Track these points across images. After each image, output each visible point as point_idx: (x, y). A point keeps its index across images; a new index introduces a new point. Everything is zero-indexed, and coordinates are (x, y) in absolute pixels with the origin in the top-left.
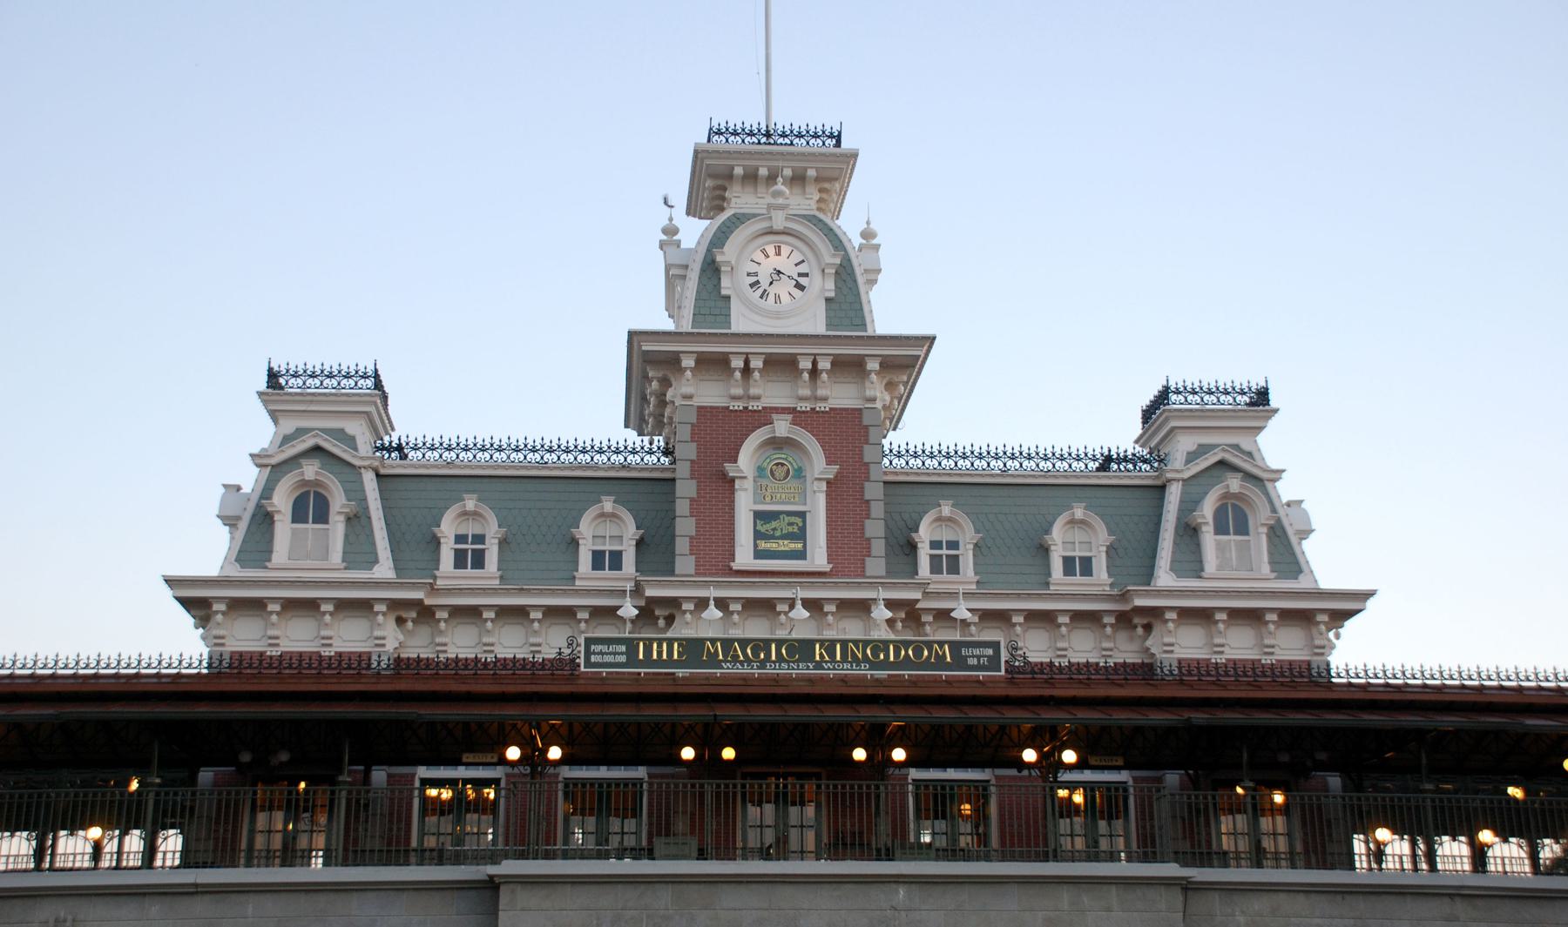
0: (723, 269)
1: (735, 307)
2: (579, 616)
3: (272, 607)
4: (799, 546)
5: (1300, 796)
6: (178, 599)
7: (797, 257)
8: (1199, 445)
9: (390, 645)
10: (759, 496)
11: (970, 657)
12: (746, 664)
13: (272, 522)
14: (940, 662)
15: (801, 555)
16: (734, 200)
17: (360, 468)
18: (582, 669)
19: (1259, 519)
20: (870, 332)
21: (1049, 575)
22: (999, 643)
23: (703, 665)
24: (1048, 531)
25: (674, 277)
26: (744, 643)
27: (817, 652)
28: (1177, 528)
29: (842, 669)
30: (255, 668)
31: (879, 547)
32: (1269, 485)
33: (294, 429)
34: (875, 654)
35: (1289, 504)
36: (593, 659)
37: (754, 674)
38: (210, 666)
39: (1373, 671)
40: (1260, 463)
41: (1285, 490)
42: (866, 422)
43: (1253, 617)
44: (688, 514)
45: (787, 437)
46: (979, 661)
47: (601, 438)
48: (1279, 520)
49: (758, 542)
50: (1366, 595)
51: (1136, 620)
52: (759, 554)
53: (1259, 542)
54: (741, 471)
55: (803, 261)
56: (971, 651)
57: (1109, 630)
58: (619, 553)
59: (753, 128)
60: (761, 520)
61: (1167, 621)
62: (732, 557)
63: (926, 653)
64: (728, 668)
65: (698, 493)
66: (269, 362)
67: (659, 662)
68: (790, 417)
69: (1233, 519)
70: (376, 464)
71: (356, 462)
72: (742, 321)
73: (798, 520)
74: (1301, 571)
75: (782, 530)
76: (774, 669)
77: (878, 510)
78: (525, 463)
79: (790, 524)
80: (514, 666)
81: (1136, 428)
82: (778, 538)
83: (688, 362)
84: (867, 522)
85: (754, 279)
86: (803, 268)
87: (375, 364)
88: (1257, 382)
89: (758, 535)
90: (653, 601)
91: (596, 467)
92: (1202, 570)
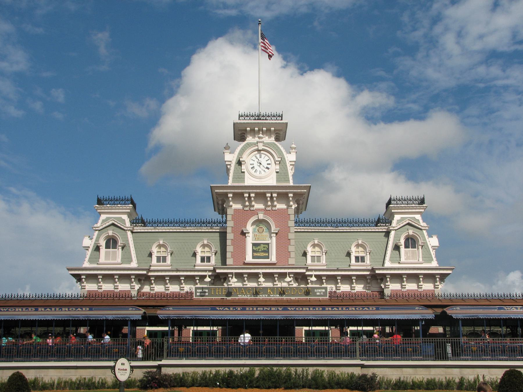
0: (242, 163)
1: (246, 174)
5: (318, 338)
7: (267, 158)
8: (401, 218)
10: (255, 237)
11: (317, 292)
12: (246, 295)
17: (126, 230)
18: (194, 297)
29: (276, 297)
30: (118, 298)
33: (106, 217)
37: (248, 298)
39: (518, 295)
44: (231, 245)
45: (263, 219)
46: (320, 294)
49: (253, 253)
52: (254, 257)
54: (248, 231)
55: (269, 160)
56: (318, 290)
57: (369, 280)
59: (275, 114)
60: (254, 246)
64: (240, 297)
65: (234, 238)
66: (98, 196)
71: (125, 228)
73: (267, 246)
75: (261, 249)
76: (255, 297)
77: (292, 242)
79: (264, 247)
80: (355, 296)
82: (261, 252)
85: (253, 166)
86: (269, 162)
87: (131, 196)
88: (421, 196)
89: (254, 251)
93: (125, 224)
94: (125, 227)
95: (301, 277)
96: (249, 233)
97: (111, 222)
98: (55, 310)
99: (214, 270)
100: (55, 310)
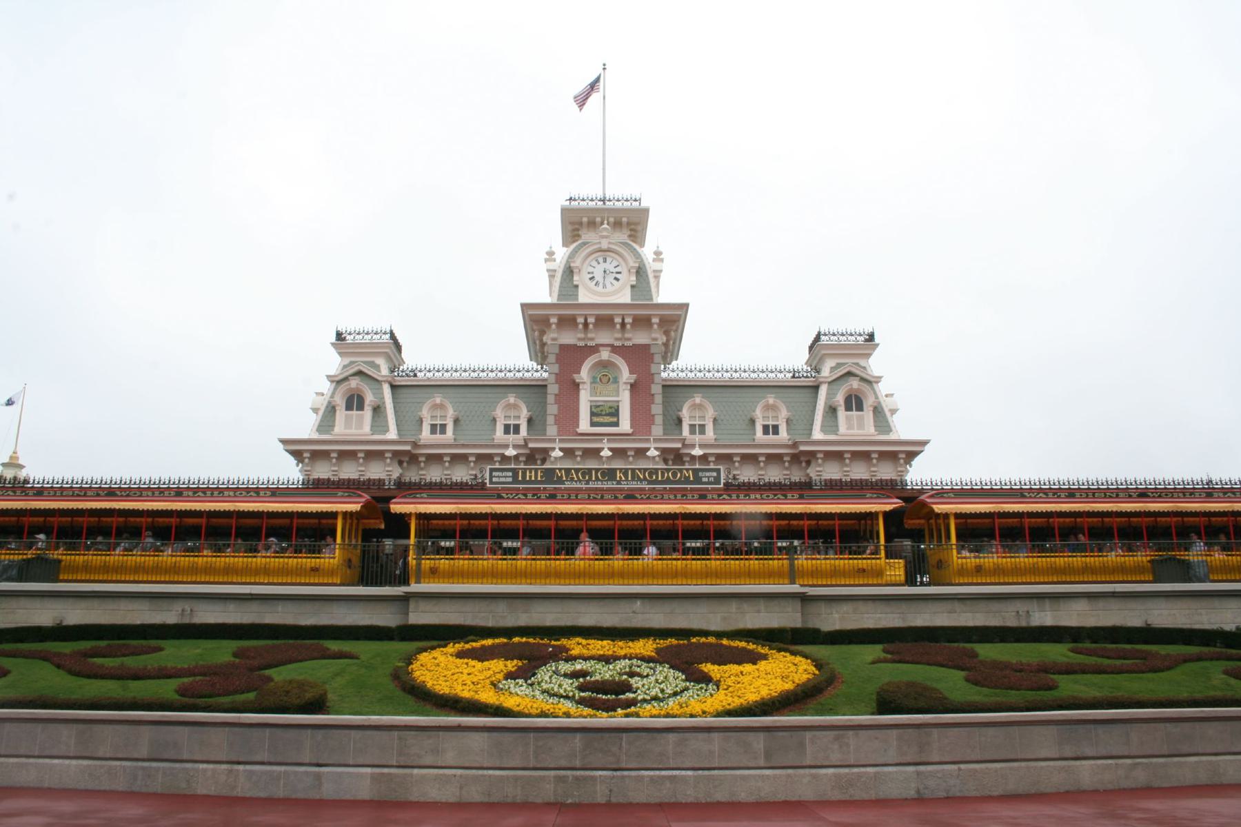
1: (581, 291)
2: (735, 459)
3: (388, 455)
4: (615, 419)
6: (287, 450)
7: (615, 263)
9: (395, 475)
13: (335, 411)
14: (687, 481)
15: (616, 424)
16: (583, 236)
18: (488, 485)
19: (868, 403)
20: (655, 301)
21: (755, 434)
22: (490, 469)
23: (555, 483)
24: (680, 410)
25: (552, 274)
26: (577, 470)
27: (618, 475)
28: (824, 409)
31: (659, 420)
32: (875, 385)
34: (651, 476)
35: (887, 396)
36: (494, 480)
38: (303, 484)
40: (870, 372)
41: (882, 388)
42: (652, 351)
43: (865, 456)
47: (519, 365)
48: (879, 403)
50: (924, 443)
51: (802, 459)
52: (593, 424)
53: (868, 415)
58: (445, 425)
61: (818, 459)
62: (578, 426)
63: (679, 475)
67: (530, 482)
68: (609, 348)
69: (854, 402)
70: (390, 379)
71: (379, 378)
72: (584, 297)
74: (891, 431)
78: (461, 378)
81: (806, 355)
83: (554, 320)
84: (653, 406)
86: (618, 269)
88: (868, 330)
89: (593, 414)
90: (533, 450)
91: (507, 380)
92: (838, 430)
93: (380, 371)
94: (379, 376)
95: (672, 457)
96: (584, 383)
97: (356, 369)
98: (738, 497)
99: (526, 445)
100: (738, 497)
